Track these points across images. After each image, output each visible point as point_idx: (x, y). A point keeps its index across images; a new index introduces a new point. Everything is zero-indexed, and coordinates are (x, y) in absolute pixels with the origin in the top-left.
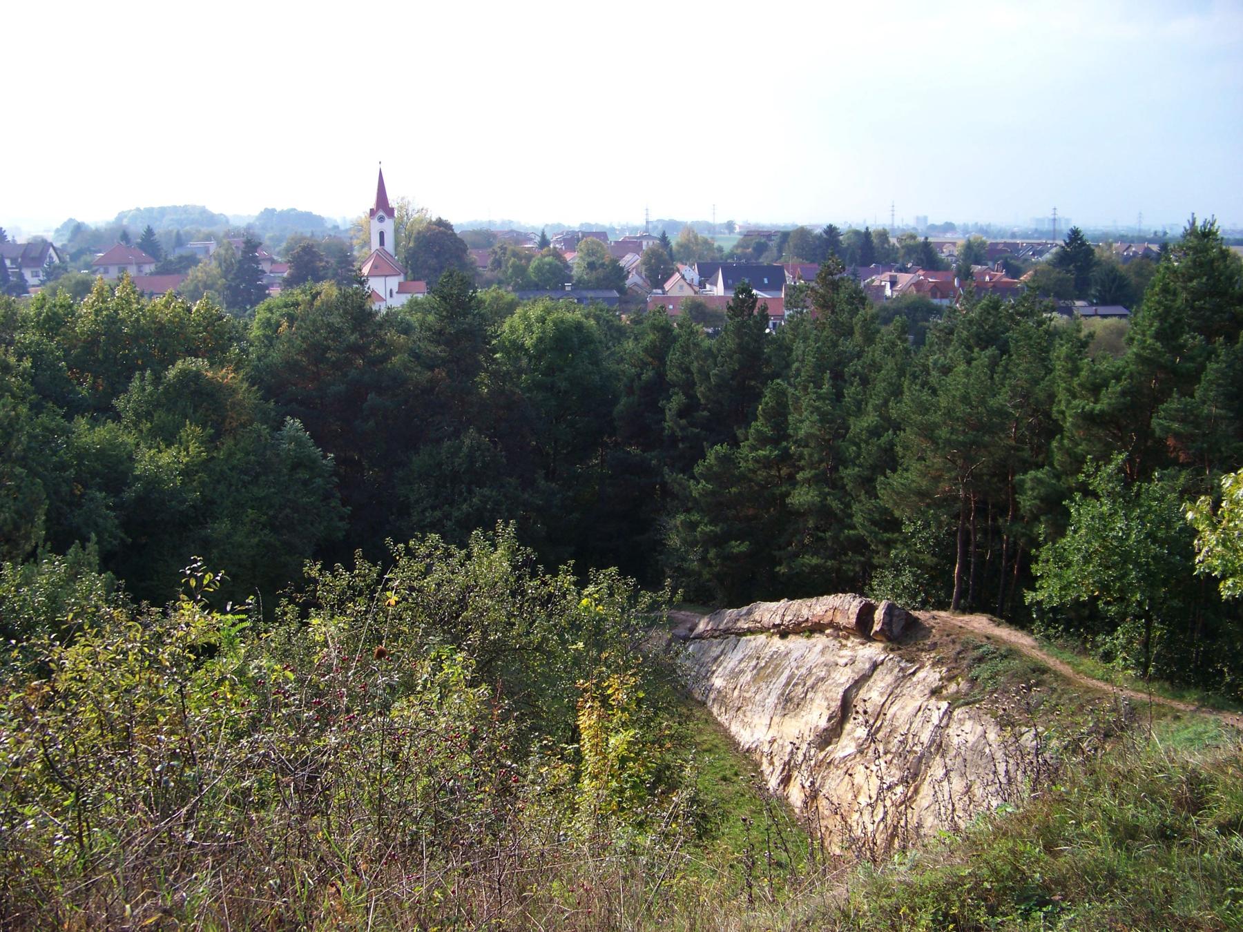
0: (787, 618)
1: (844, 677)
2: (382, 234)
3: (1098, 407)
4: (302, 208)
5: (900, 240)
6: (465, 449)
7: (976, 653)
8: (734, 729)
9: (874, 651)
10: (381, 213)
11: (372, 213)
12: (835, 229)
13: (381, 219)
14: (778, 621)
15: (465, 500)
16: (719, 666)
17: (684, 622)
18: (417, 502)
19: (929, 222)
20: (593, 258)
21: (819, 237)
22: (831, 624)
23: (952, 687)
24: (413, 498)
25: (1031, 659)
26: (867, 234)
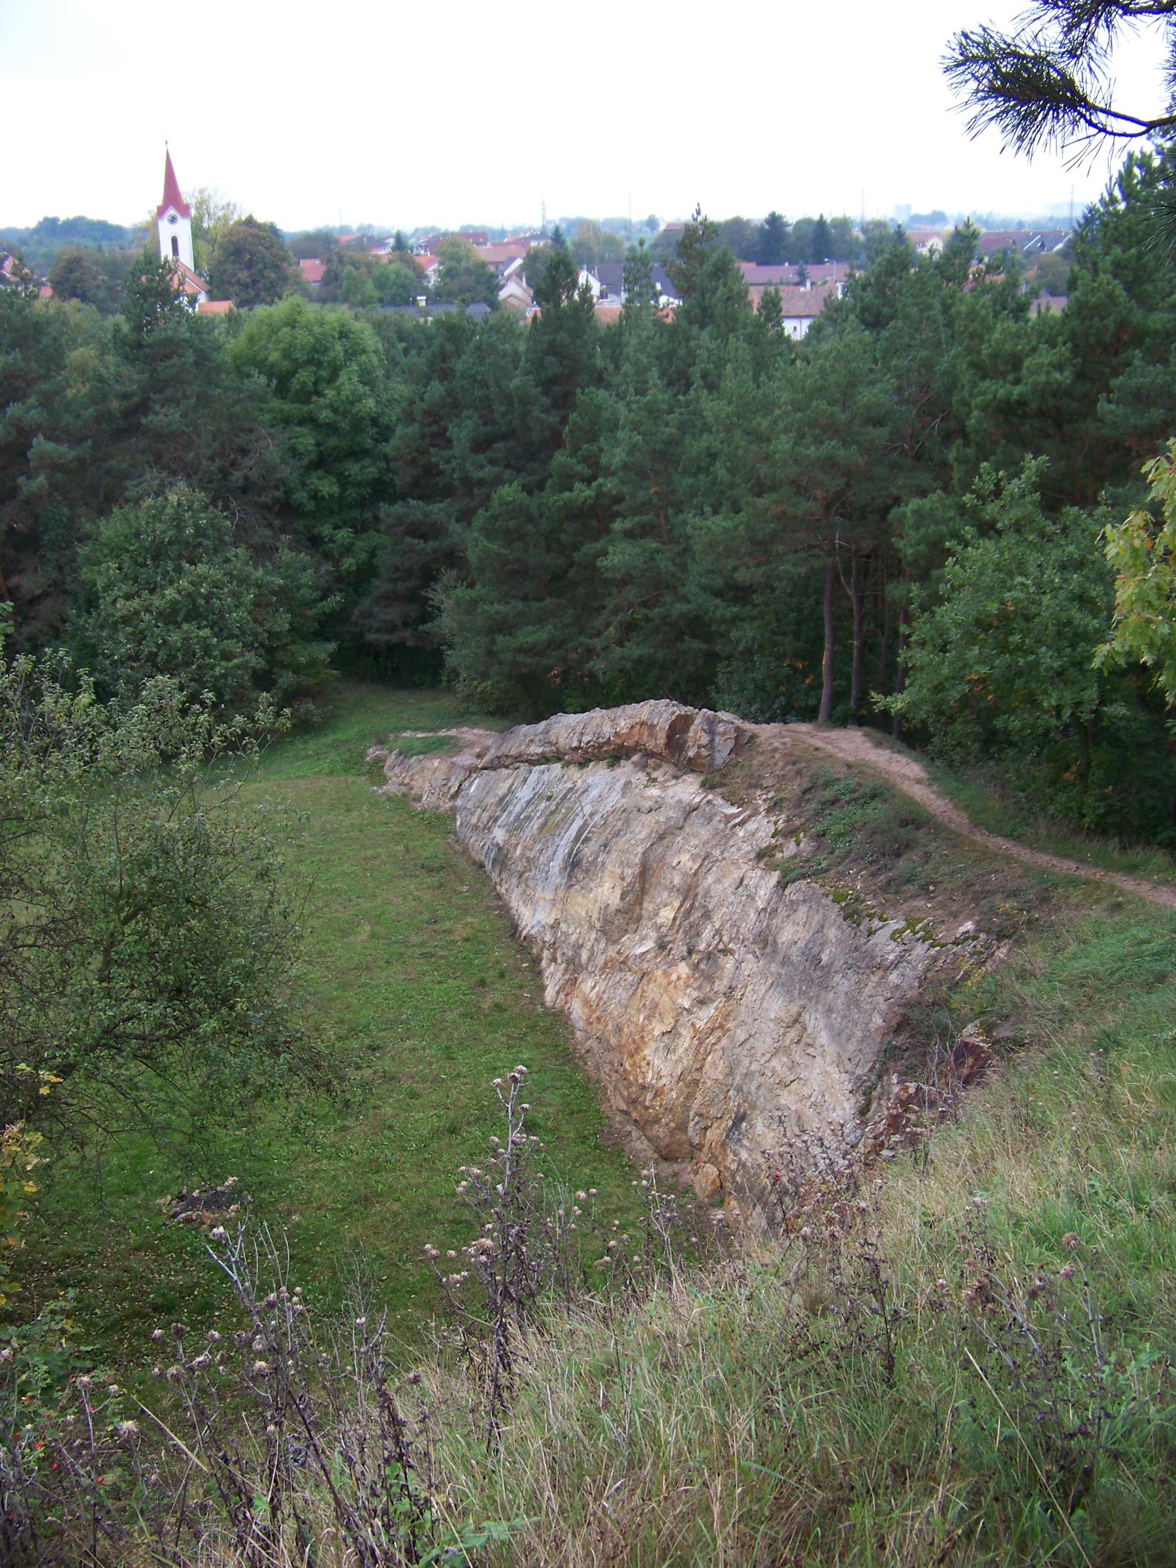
0: (585, 739)
1: (643, 829)
2: (174, 241)
3: (1017, 390)
4: (94, 214)
5: (864, 230)
6: (170, 511)
7: (828, 794)
8: (515, 902)
9: (688, 789)
10: (172, 212)
11: (161, 211)
12: (780, 217)
13: (173, 220)
14: (575, 744)
15: (171, 582)
16: (504, 810)
17: (471, 745)
18: (107, 588)
19: (913, 212)
20: (454, 263)
21: (761, 230)
22: (635, 749)
23: (790, 848)
24: (101, 583)
25: (910, 801)
26: (821, 223)
